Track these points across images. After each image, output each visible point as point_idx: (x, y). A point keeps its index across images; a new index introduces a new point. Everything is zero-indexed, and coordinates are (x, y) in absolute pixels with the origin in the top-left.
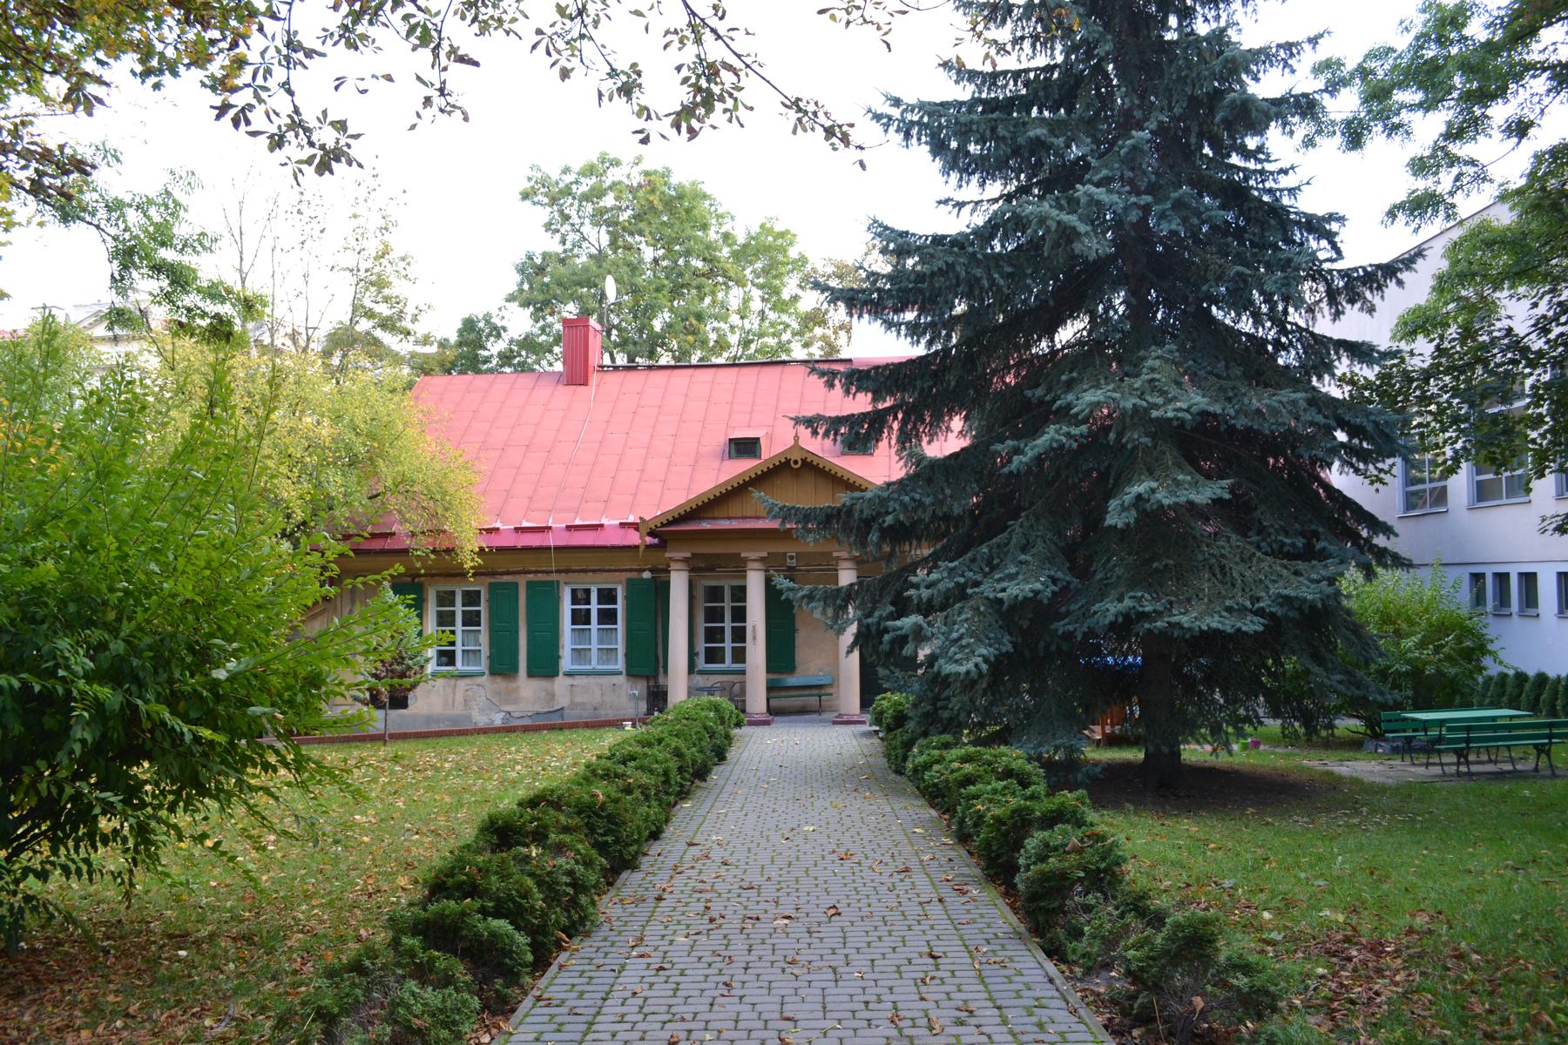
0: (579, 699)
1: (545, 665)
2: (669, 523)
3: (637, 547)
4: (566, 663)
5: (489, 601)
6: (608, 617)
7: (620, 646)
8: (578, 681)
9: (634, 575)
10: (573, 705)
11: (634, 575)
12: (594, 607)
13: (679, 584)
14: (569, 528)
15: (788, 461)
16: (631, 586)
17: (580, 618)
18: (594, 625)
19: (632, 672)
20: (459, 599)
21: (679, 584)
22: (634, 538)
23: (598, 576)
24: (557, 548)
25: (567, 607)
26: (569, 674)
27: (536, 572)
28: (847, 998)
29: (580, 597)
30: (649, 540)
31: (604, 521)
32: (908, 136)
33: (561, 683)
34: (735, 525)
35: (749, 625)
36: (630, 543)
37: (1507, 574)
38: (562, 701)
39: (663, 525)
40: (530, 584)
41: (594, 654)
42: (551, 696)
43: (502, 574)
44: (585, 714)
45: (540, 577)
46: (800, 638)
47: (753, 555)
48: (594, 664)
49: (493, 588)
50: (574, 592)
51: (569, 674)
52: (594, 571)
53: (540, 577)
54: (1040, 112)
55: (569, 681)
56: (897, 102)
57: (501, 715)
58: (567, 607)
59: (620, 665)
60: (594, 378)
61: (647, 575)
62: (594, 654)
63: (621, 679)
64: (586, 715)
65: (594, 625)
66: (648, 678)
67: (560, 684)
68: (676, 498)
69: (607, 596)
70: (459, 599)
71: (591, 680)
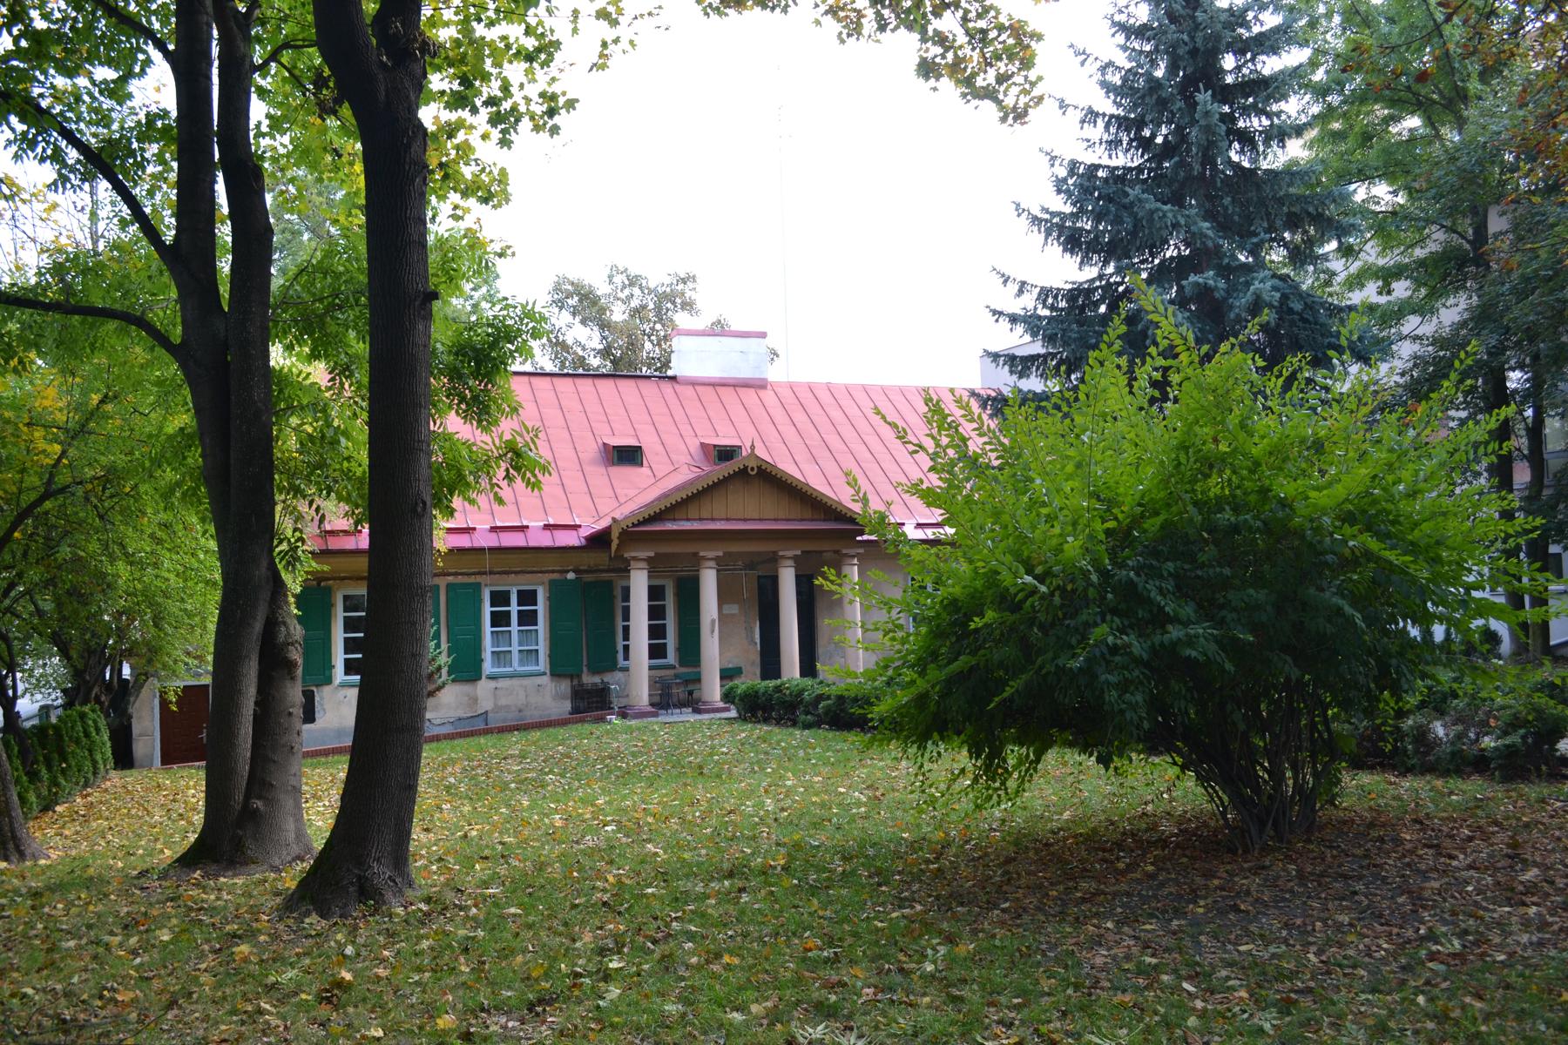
0: (503, 702)
2: (640, 523)
4: (488, 667)
6: (528, 618)
7: (543, 647)
8: (502, 683)
9: (555, 576)
10: (497, 708)
11: (555, 576)
12: (514, 608)
13: (639, 583)
14: (547, 527)
15: (746, 467)
17: (500, 619)
18: (514, 627)
19: (556, 673)
20: (514, 599)
21: (639, 583)
23: (521, 578)
24: (490, 549)
25: (487, 609)
26: (492, 678)
27: (456, 574)
29: (500, 598)
31: (531, 524)
32: (1048, 234)
33: (484, 686)
34: (696, 526)
35: (632, 624)
38: (486, 704)
40: (449, 586)
41: (515, 656)
42: (474, 700)
45: (460, 579)
47: (790, 553)
48: (516, 666)
50: (346, 598)
51: (492, 678)
52: (516, 573)
53: (460, 579)
55: (493, 684)
56: (1047, 211)
58: (487, 609)
59: (543, 663)
61: (571, 576)
62: (515, 656)
63: (545, 680)
64: (511, 718)
65: (514, 627)
66: (571, 677)
67: (483, 687)
69: (527, 597)
70: (514, 599)
71: (515, 682)
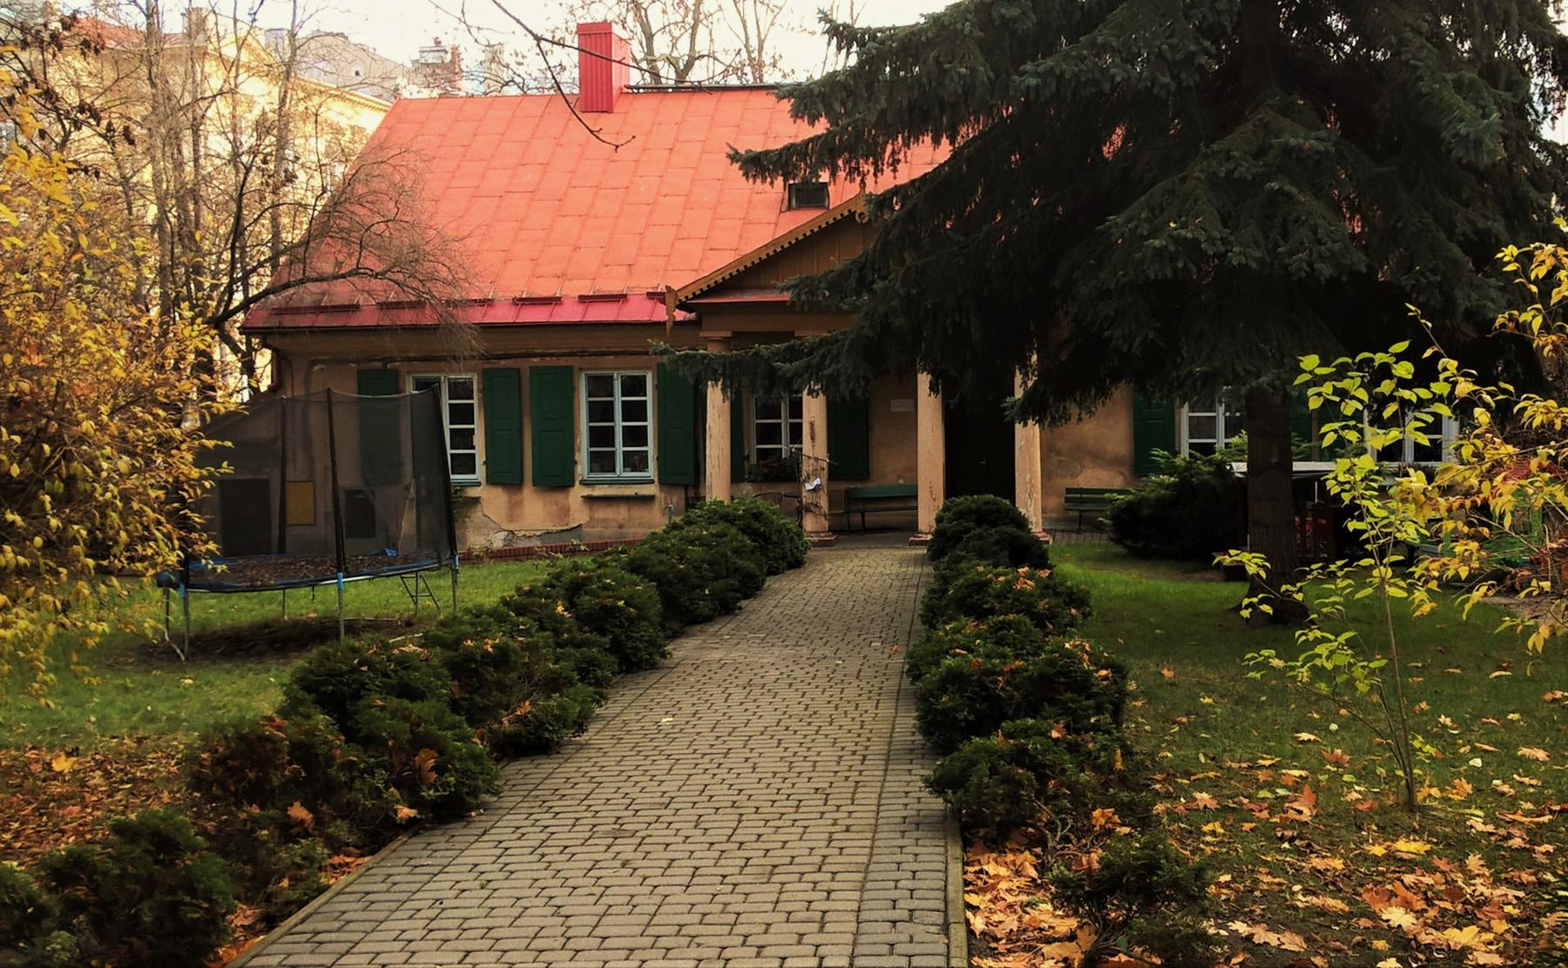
1: (556, 479)
2: (704, 294)
3: (664, 323)
4: (582, 468)
5: (656, 387)
16: (661, 373)
20: (618, 386)
22: (660, 314)
27: (542, 355)
28: (894, 866)
29: (601, 385)
30: (680, 315)
36: (655, 319)
37: (473, 472)
39: (695, 296)
43: (499, 357)
44: (609, 532)
46: (877, 435)
49: (486, 376)
52: (616, 354)
53: (554, 362)
54: (1350, 44)
57: (503, 535)
60: (620, 106)
66: (686, 487)
68: (720, 261)
69: (634, 386)
